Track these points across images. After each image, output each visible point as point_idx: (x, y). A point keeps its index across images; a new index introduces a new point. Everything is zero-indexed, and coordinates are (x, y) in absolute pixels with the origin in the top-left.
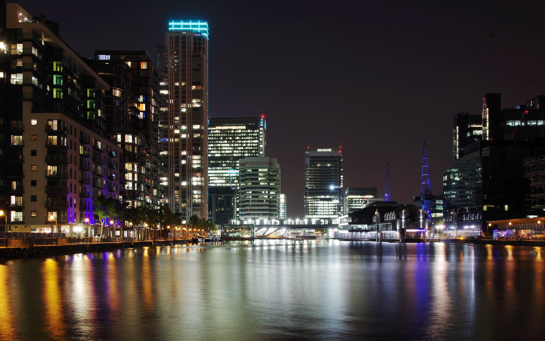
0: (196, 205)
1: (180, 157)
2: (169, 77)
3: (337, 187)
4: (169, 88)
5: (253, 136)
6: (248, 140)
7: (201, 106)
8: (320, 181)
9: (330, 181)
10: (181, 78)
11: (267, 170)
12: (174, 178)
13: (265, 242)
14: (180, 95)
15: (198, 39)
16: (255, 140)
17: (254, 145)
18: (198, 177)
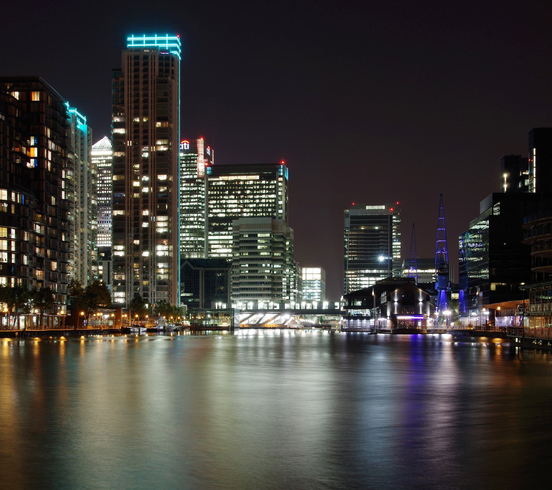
0: (161, 283)
1: (141, 218)
2: (126, 111)
3: (387, 258)
4: (126, 125)
5: (269, 189)
6: (262, 194)
7: (169, 150)
8: (365, 250)
9: (378, 250)
10: (141, 111)
11: (268, 235)
12: (133, 247)
13: (261, 332)
14: (141, 135)
15: (166, 59)
16: (274, 195)
17: (270, 201)
18: (164, 245)
